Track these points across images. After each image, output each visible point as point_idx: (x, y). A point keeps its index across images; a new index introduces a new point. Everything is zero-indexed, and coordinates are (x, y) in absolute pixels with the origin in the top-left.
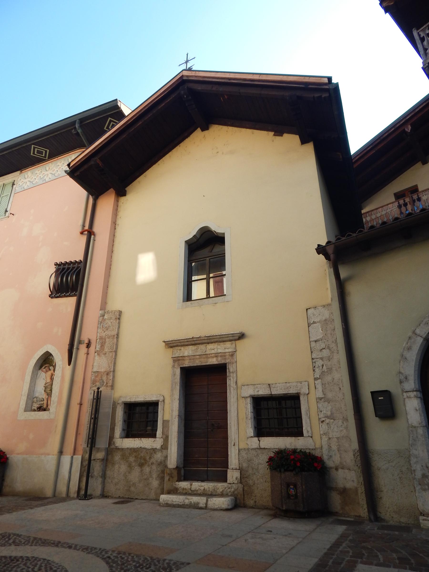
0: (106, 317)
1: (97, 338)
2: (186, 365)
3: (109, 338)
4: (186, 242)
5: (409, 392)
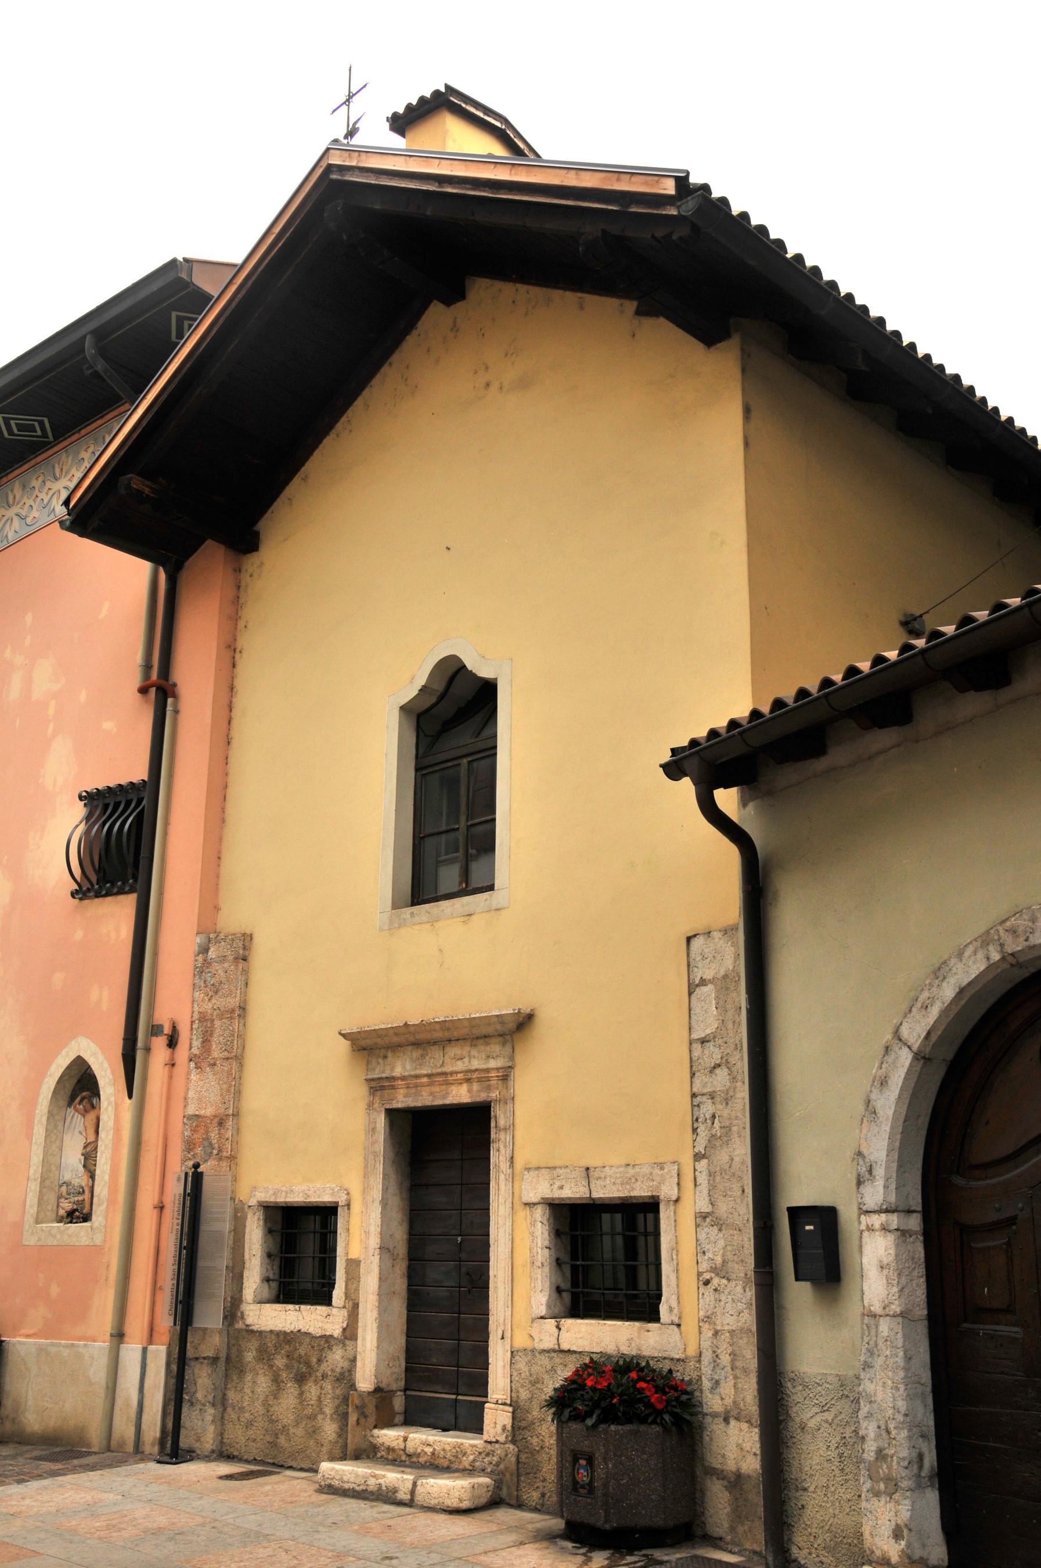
0: (212, 954)
1: (192, 1016)
2: (398, 1102)
3: (221, 1017)
4: (403, 709)
5: (872, 1214)
